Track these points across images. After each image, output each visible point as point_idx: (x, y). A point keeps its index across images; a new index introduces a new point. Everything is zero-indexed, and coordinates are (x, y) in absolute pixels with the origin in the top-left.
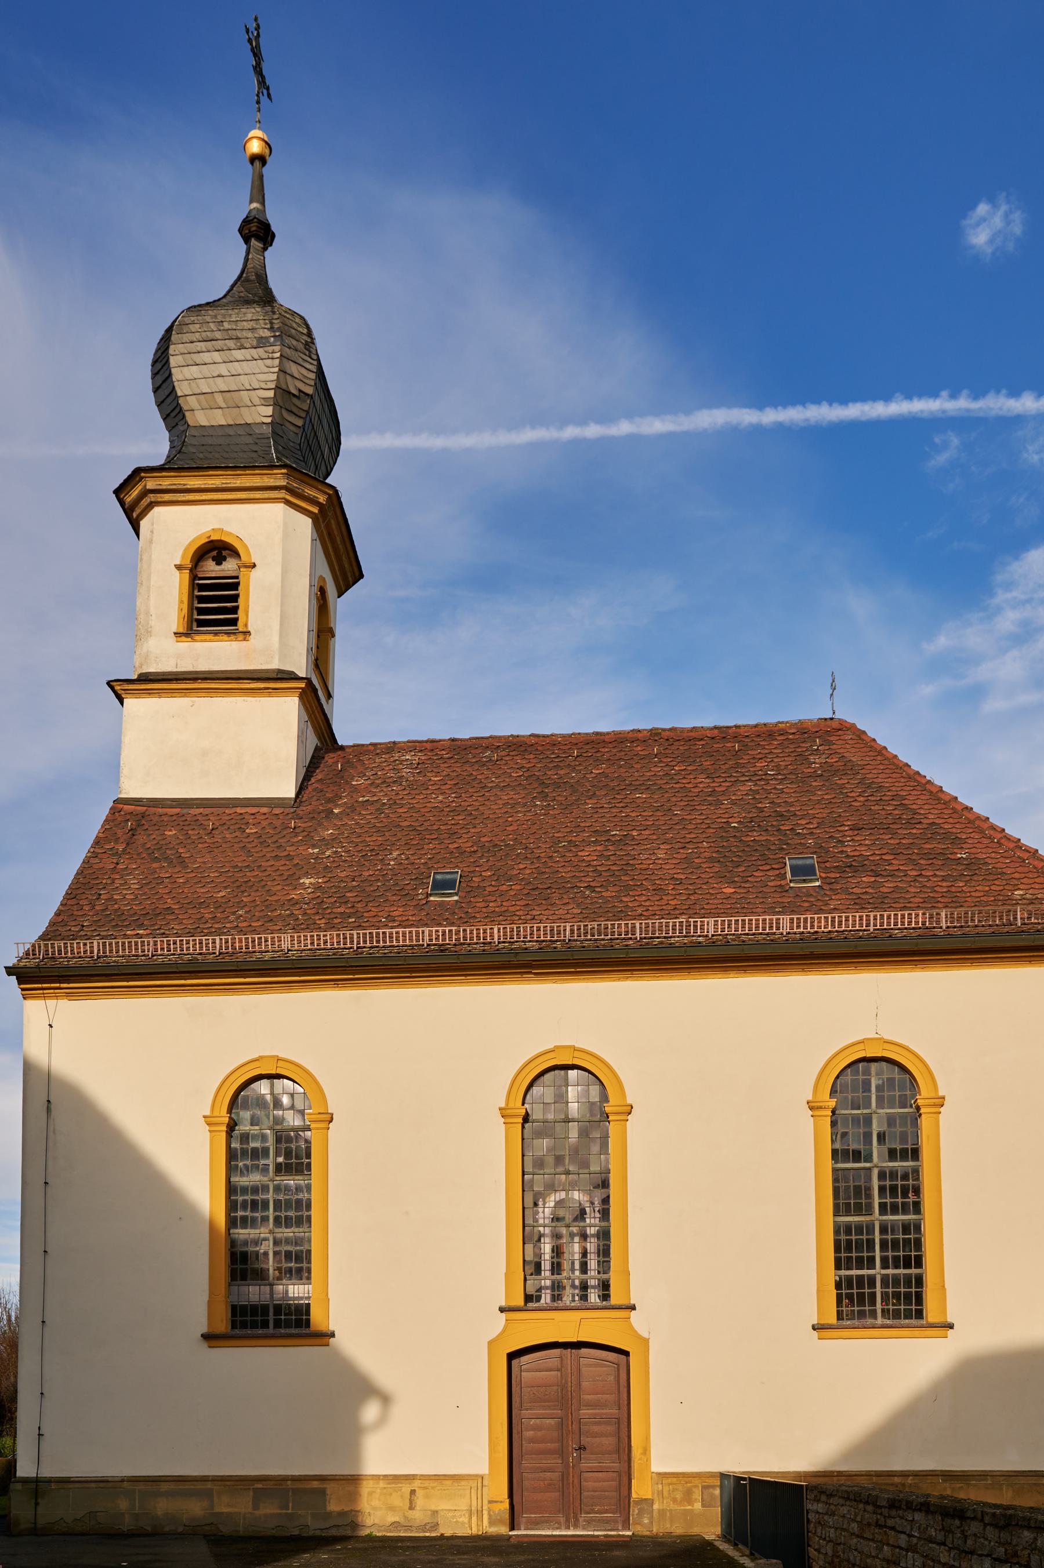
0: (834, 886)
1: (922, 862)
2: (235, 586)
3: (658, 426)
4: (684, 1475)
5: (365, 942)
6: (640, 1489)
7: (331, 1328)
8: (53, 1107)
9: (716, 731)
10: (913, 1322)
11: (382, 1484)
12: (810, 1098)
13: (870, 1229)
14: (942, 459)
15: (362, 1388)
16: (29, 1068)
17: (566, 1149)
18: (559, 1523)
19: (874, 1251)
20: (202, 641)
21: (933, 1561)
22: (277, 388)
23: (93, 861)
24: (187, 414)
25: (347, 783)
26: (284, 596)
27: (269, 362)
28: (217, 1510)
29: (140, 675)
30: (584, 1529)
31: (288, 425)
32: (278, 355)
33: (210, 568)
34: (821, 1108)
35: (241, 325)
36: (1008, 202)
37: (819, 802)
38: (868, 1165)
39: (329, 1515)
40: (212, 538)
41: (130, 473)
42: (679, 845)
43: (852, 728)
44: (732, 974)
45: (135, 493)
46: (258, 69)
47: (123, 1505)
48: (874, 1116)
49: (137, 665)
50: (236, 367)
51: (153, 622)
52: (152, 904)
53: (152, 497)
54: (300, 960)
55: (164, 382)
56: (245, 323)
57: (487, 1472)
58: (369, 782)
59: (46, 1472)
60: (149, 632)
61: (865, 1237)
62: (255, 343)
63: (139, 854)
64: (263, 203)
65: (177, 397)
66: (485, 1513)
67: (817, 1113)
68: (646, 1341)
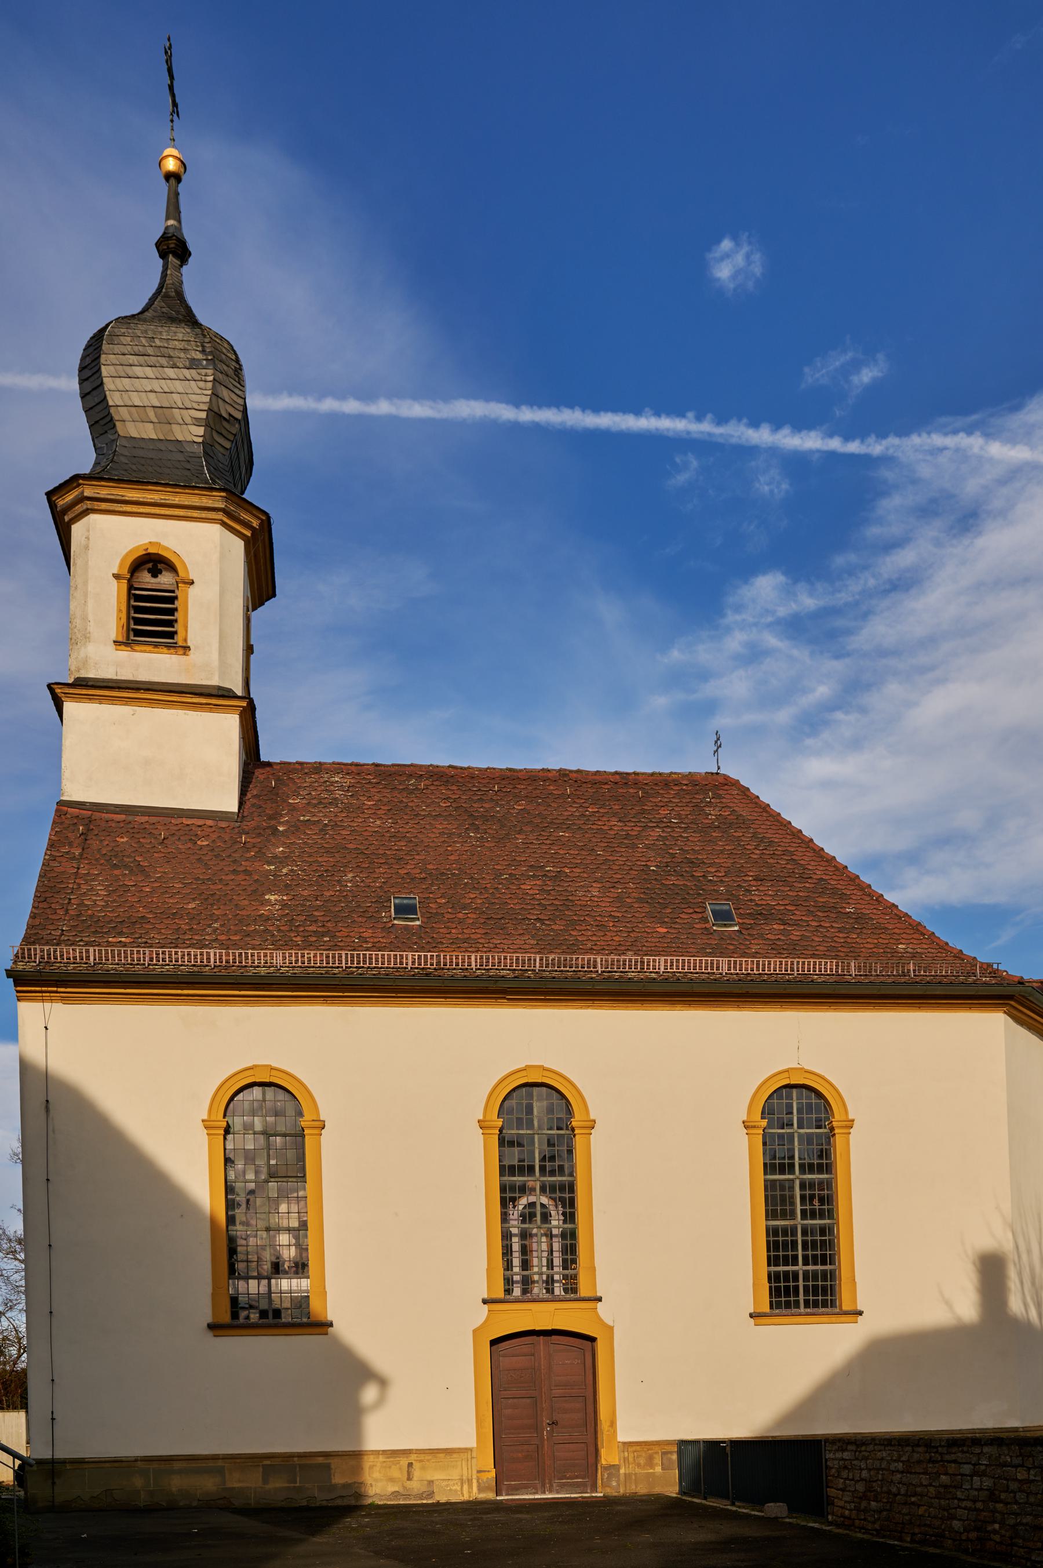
0: (751, 932)
1: (819, 914)
2: (172, 600)
3: (419, 410)
4: (646, 1443)
5: (352, 962)
6: (608, 1456)
7: (330, 1318)
8: (51, 1107)
9: (617, 777)
10: (829, 1310)
11: (381, 1458)
12: (745, 1118)
13: (794, 1232)
14: (682, 478)
15: (361, 1373)
16: (26, 1068)
17: (537, 1154)
18: (536, 1489)
19: (797, 1250)
20: (141, 651)
21: (1005, 1479)
22: (210, 410)
23: (52, 864)
24: (117, 424)
25: (285, 801)
26: (222, 616)
27: (201, 384)
28: (229, 1485)
29: (77, 679)
30: (558, 1493)
31: (217, 446)
32: (211, 378)
33: (146, 579)
34: (754, 1127)
35: (172, 344)
36: (750, 243)
37: (722, 852)
38: (791, 1177)
39: (334, 1487)
40: (150, 551)
41: (68, 478)
42: (608, 885)
43: (736, 783)
44: (679, 1007)
45: (70, 497)
46: (171, 88)
47: (138, 1482)
48: (796, 1135)
49: (73, 668)
50: (165, 385)
51: (92, 627)
52: (120, 910)
53: (88, 504)
54: (295, 976)
55: (94, 389)
56: (177, 343)
57: (475, 1445)
58: (304, 801)
59: (60, 1455)
60: (87, 637)
61: (789, 1239)
62: (187, 364)
63: (96, 860)
64: (179, 222)
65: (108, 406)
66: (475, 1481)
67: (751, 1131)
68: (611, 1328)
